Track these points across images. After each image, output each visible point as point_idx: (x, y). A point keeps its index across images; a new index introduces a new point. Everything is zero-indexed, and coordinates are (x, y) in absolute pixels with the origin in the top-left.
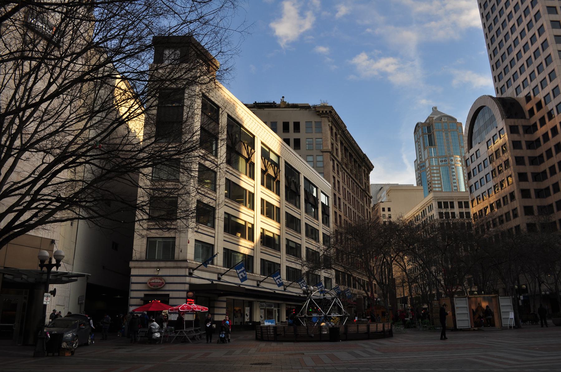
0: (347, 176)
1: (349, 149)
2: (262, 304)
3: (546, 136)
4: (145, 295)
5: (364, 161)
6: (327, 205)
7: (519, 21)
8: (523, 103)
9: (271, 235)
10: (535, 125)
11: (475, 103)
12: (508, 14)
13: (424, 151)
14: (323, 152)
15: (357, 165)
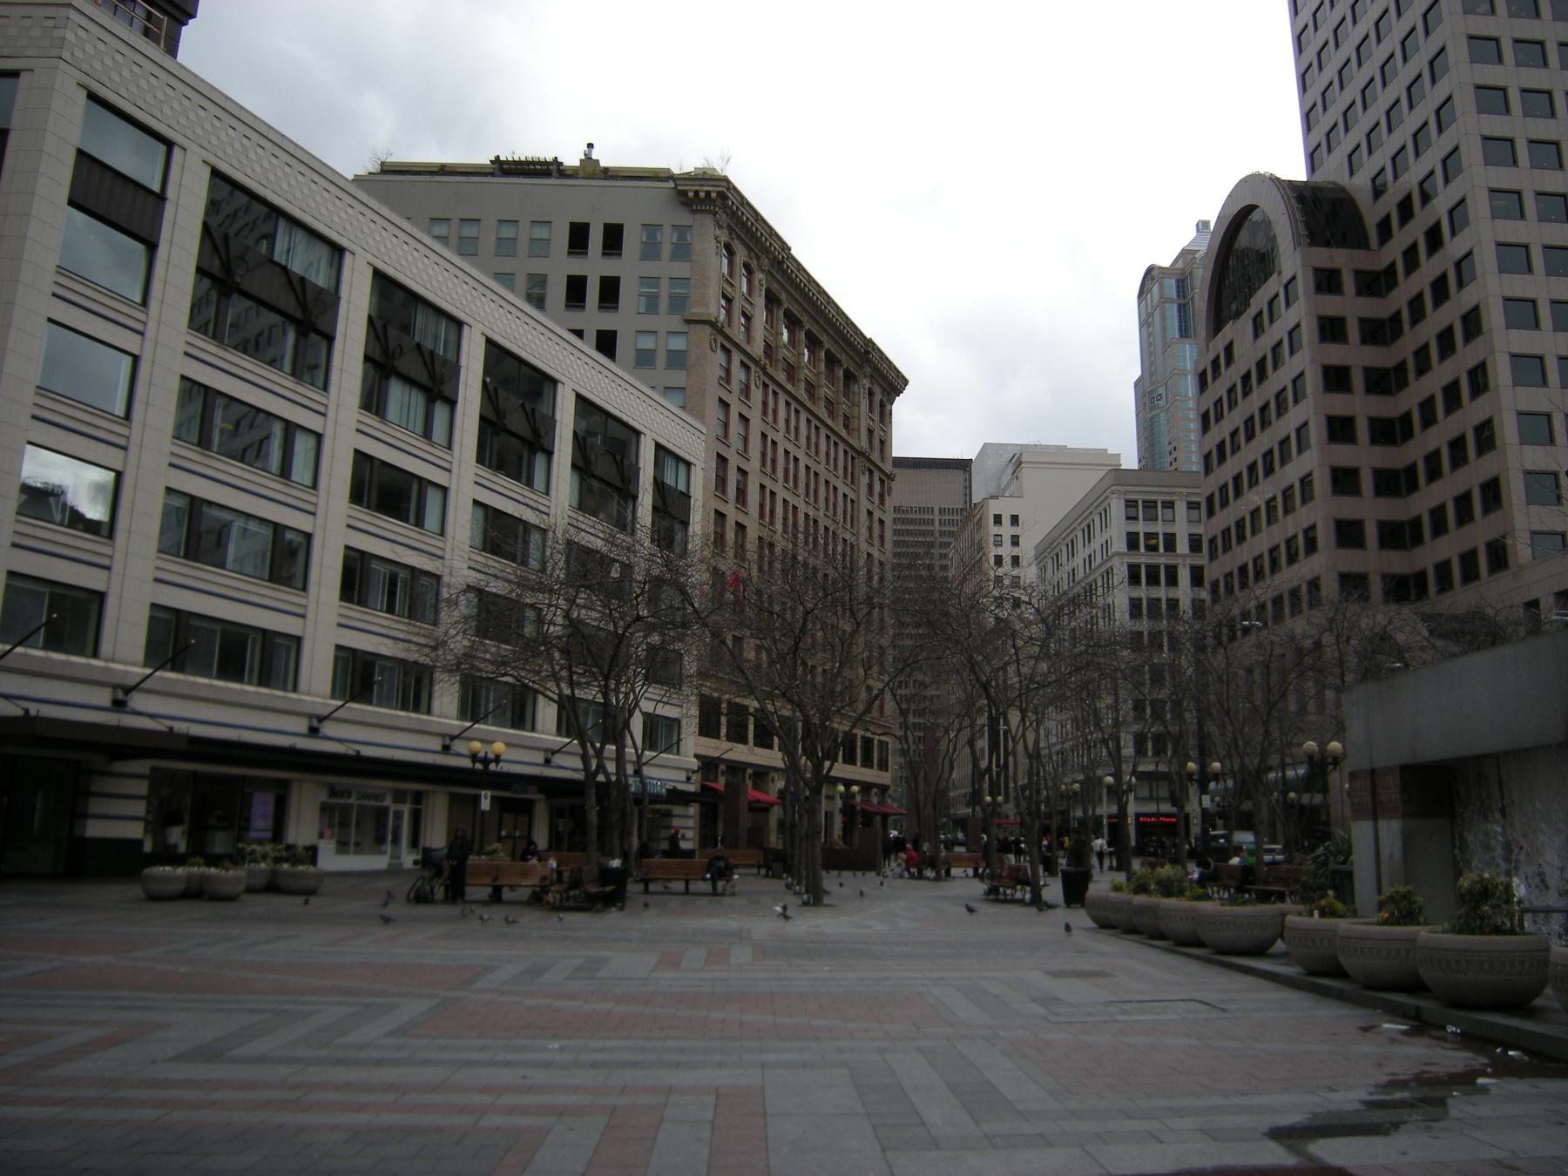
5: (869, 361)
8: (1363, 199)
14: (688, 322)
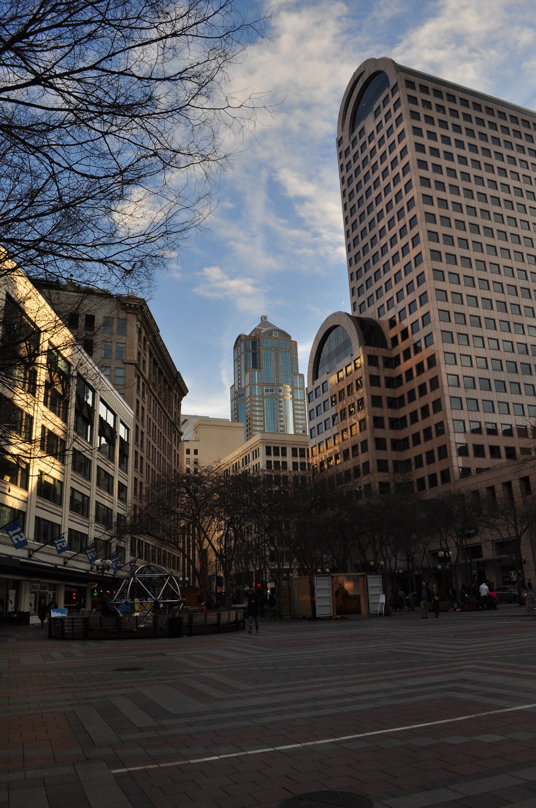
0: (154, 401)
1: (158, 362)
2: (35, 585)
3: (409, 373)
5: (177, 382)
6: (126, 440)
7: (391, 223)
8: (385, 327)
9: (51, 481)
10: (397, 358)
11: (327, 320)
12: (378, 212)
14: (125, 363)
15: (167, 387)
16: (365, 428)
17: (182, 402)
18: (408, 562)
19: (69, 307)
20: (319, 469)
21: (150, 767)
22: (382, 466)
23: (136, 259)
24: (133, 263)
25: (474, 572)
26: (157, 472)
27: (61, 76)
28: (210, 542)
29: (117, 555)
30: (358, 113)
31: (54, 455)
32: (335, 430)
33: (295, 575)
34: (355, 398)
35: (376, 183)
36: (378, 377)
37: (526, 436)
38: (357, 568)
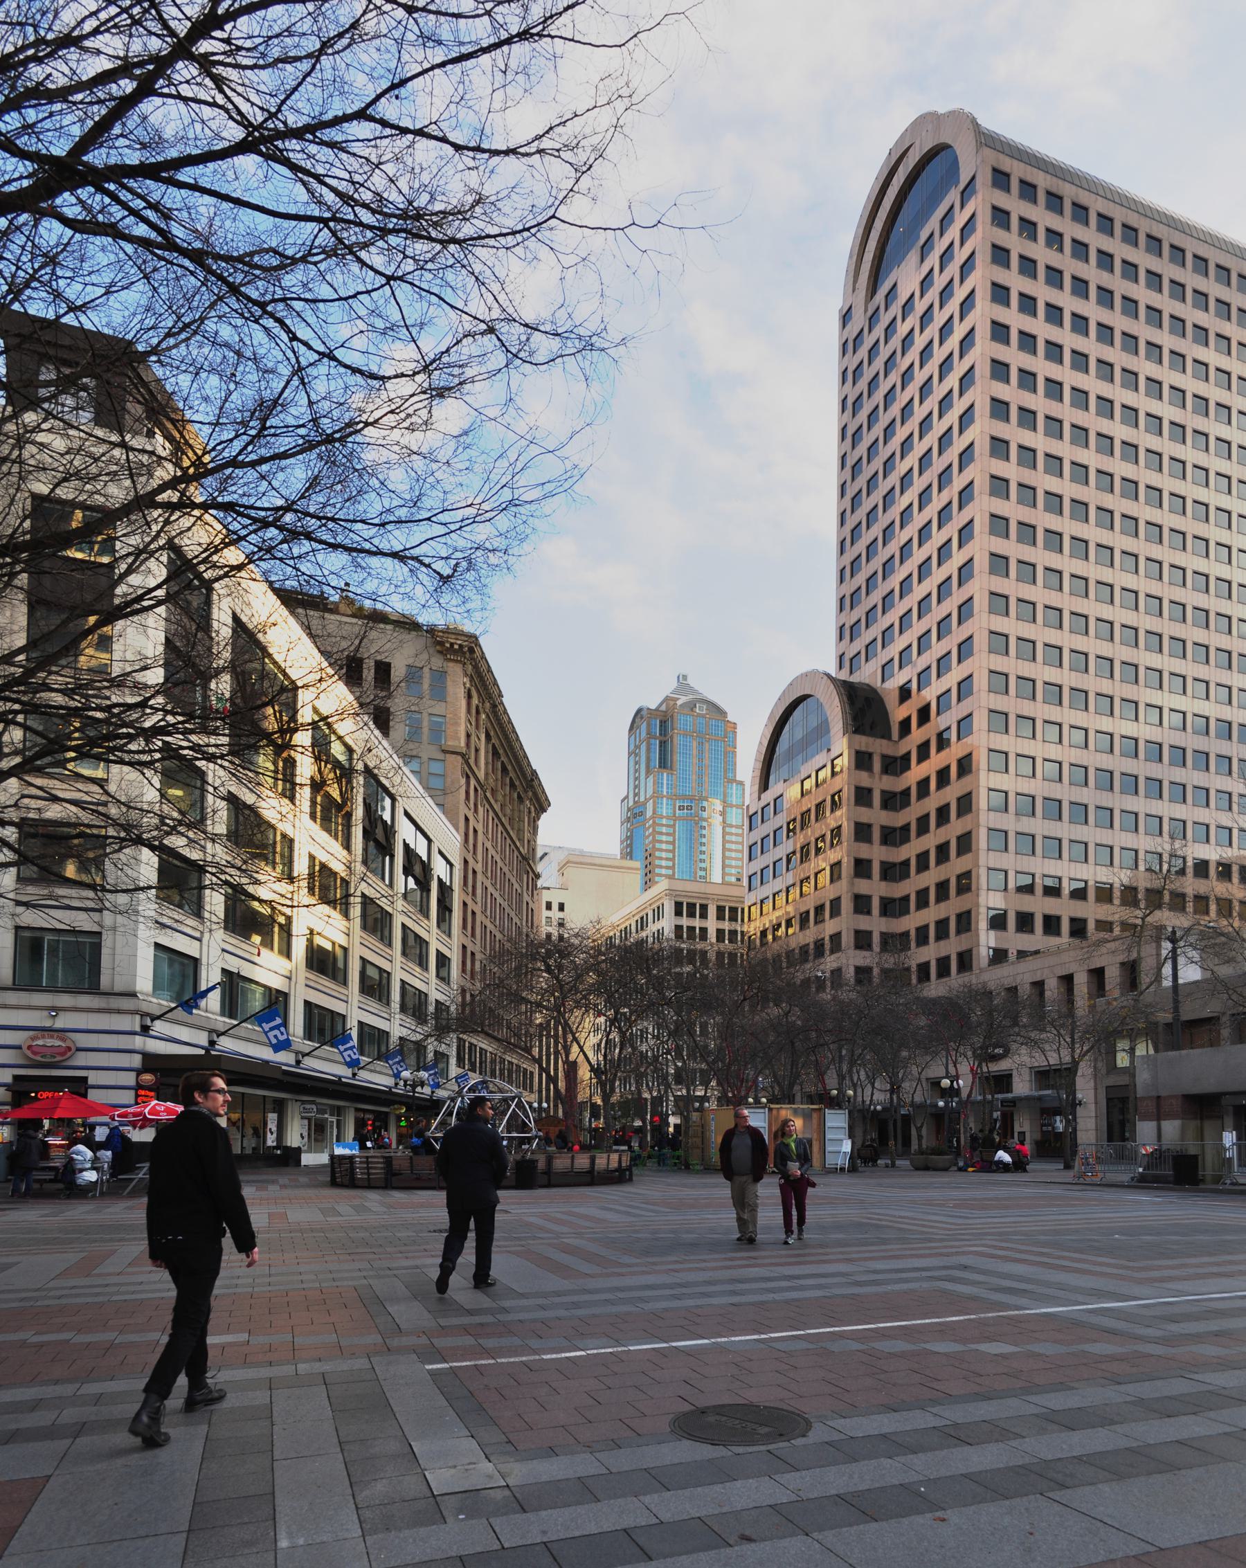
1: (501, 751)
2: (308, 1106)
3: (923, 785)
4: (16, 1078)
5: (532, 787)
7: (924, 498)
8: (891, 701)
9: (328, 946)
13: (647, 777)
14: (445, 752)
15: (516, 795)
16: (839, 877)
17: (541, 823)
18: (891, 1094)
19: (344, 644)
20: (758, 942)
21: (483, 1362)
22: (862, 940)
23: (459, 555)
24: (453, 562)
25: (996, 1115)
26: (499, 936)
27: (298, 134)
28: (581, 1048)
29: (435, 1065)
30: (888, 249)
31: (331, 903)
32: (790, 878)
33: (712, 1105)
34: (827, 825)
35: (907, 410)
36: (870, 791)
37: (1110, 900)
38: (810, 1099)
